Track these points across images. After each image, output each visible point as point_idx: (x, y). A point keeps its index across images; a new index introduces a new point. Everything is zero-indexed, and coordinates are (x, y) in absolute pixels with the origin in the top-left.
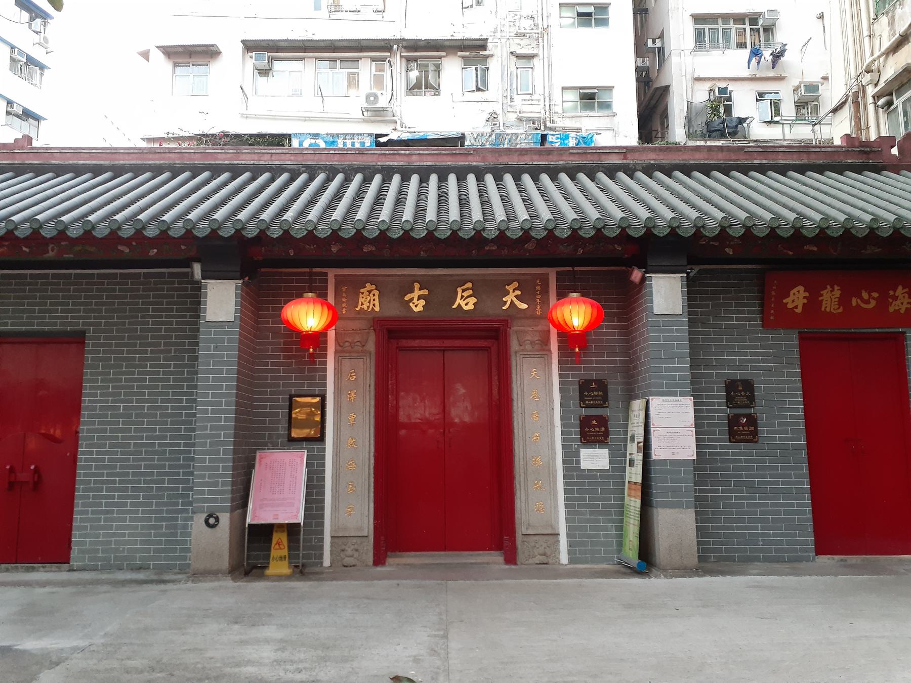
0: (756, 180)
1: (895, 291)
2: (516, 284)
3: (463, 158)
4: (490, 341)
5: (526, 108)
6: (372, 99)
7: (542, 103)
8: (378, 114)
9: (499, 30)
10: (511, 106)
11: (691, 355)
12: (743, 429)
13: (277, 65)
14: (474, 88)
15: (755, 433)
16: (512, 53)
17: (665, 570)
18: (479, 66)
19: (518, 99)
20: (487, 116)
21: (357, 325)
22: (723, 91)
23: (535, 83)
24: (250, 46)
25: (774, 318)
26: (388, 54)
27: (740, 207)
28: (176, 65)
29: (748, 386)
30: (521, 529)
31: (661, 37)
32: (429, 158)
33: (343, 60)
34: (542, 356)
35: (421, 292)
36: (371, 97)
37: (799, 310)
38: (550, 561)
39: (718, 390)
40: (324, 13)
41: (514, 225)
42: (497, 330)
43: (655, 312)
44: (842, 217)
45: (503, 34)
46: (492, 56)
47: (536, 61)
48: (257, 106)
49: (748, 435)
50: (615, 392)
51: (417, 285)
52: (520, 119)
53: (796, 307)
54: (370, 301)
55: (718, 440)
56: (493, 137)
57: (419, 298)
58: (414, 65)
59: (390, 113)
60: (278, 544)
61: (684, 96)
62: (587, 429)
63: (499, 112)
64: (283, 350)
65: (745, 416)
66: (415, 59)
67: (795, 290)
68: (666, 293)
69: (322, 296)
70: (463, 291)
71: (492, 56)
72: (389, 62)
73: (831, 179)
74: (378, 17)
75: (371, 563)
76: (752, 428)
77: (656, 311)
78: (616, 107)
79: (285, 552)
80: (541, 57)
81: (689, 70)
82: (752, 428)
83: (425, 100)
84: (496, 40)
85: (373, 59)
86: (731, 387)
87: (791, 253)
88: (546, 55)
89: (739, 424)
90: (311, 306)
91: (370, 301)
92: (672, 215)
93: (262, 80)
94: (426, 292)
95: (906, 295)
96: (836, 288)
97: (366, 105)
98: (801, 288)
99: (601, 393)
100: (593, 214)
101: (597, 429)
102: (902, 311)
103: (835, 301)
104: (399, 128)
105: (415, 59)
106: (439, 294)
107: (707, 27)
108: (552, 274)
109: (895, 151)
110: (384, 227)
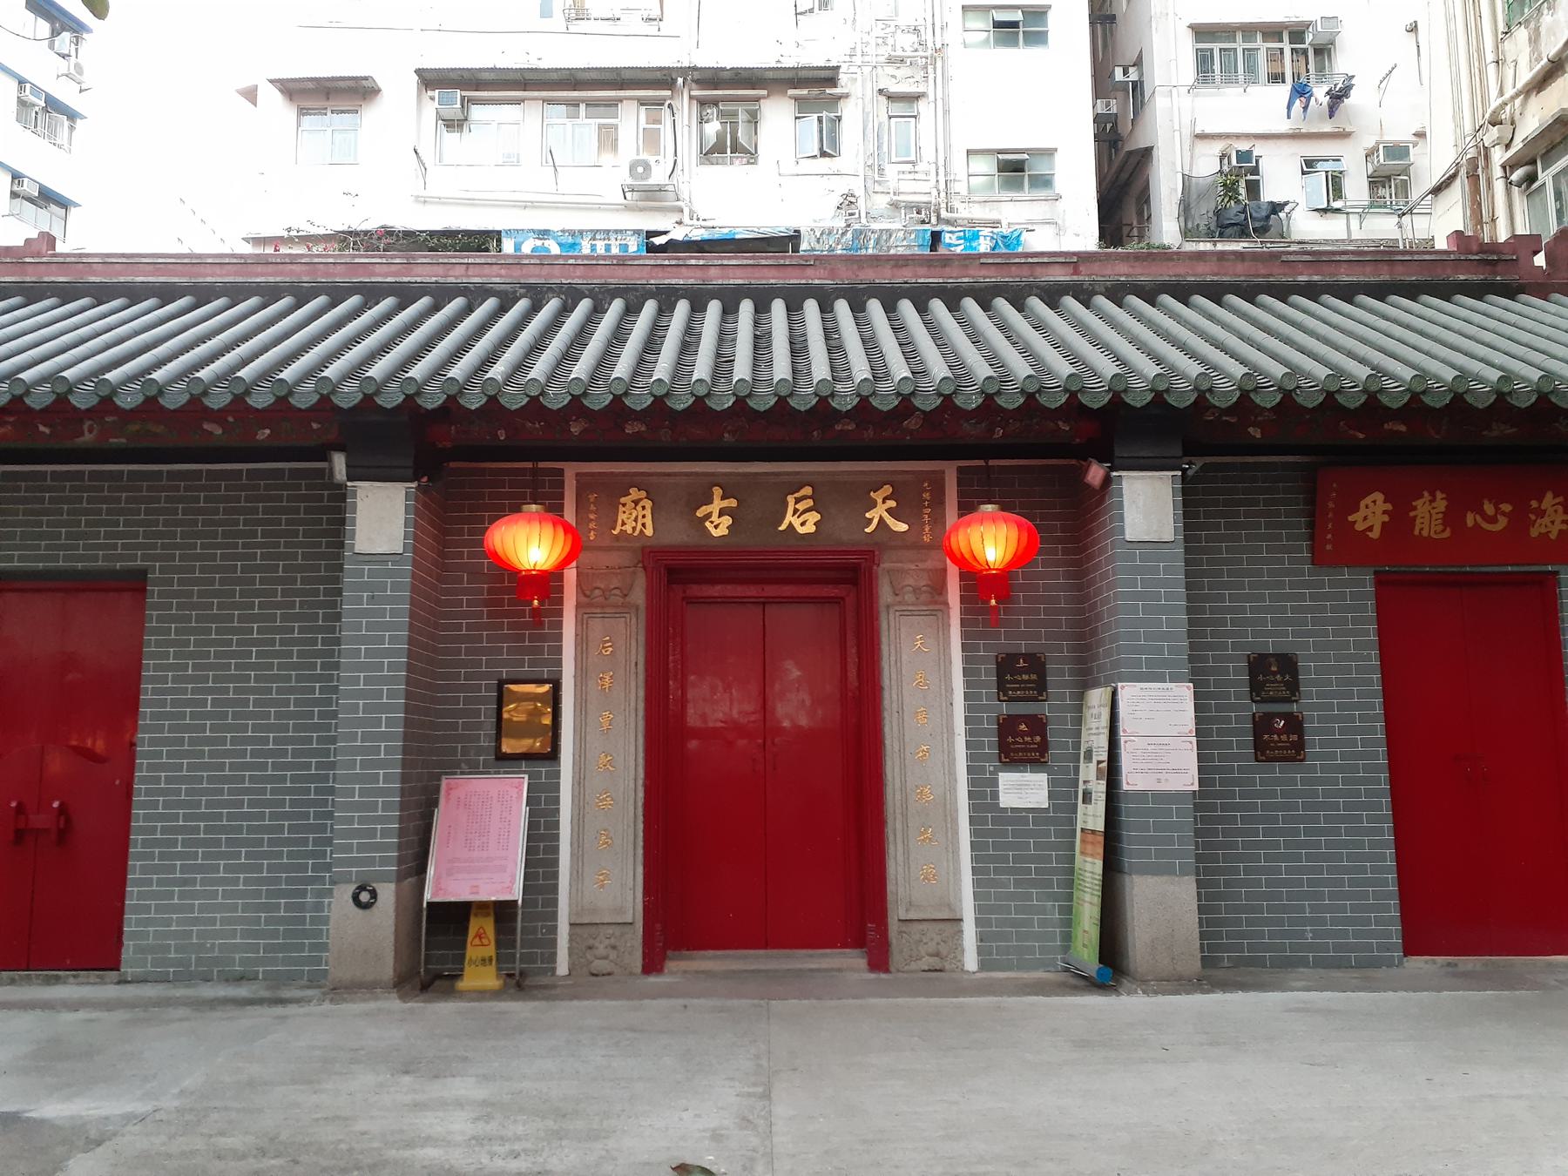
0: (1301, 309)
1: (1540, 501)
2: (888, 490)
3: (797, 272)
4: (844, 587)
5: (906, 186)
6: (640, 170)
7: (933, 177)
8: (650, 196)
9: (859, 53)
10: (879, 183)
11: (1189, 611)
12: (1279, 739)
13: (477, 112)
14: (816, 152)
15: (1299, 746)
16: (881, 91)
17: (1144, 982)
18: (824, 114)
19: (891, 171)
20: (838, 200)
21: (614, 559)
22: (1244, 156)
23: (921, 143)
24: (430, 80)
25: (1333, 547)
26: (668, 93)
27: (1274, 356)
28: (302, 112)
29: (1288, 664)
30: (897, 911)
31: (1138, 63)
32: (738, 272)
33: (590, 104)
34: (932, 613)
35: (725, 503)
36: (639, 168)
37: (1375, 534)
38: (947, 967)
39: (1236, 671)
40: (558, 22)
41: (884, 387)
42: (855, 568)
43: (1128, 538)
44: (1449, 374)
45: (866, 59)
46: (847, 96)
47: (922, 105)
48: (442, 182)
49: (1287, 748)
50: (1059, 674)
51: (717, 492)
52: (895, 205)
53: (1370, 529)
54: (636, 519)
55: (1236, 757)
56: (849, 235)
57: (722, 513)
58: (712, 111)
59: (671, 195)
60: (479, 936)
61: (1178, 166)
62: (1010, 739)
63: (859, 192)
64: (487, 603)
65: (1282, 716)
66: (715, 102)
67: (1368, 500)
68: (1146, 505)
69: (554, 509)
70: (798, 501)
71: (847, 96)
72: (670, 106)
73: (1430, 308)
74: (651, 29)
75: (639, 969)
76: (1294, 737)
77: (1130, 535)
78: (1060, 184)
79: (490, 951)
80: (931, 97)
81: (1186, 120)
82: (1294, 737)
83: (731, 173)
84: (853, 69)
85: (642, 102)
86: (1259, 666)
87: (1361, 436)
88: (939, 95)
89: (1272, 731)
90: (536, 527)
91: (636, 519)
92: (1157, 370)
93: (451, 138)
94: (733, 503)
95: (1560, 508)
96: (1439, 495)
97: (629, 181)
98: (1379, 496)
99: (1034, 677)
100: (1021, 369)
101: (1028, 739)
102: (1553, 536)
103: (1438, 518)
104: (686, 220)
105: (715, 102)
106: (755, 507)
107: (1216, 47)
108: (950, 471)
109: (1540, 260)
110: (660, 391)
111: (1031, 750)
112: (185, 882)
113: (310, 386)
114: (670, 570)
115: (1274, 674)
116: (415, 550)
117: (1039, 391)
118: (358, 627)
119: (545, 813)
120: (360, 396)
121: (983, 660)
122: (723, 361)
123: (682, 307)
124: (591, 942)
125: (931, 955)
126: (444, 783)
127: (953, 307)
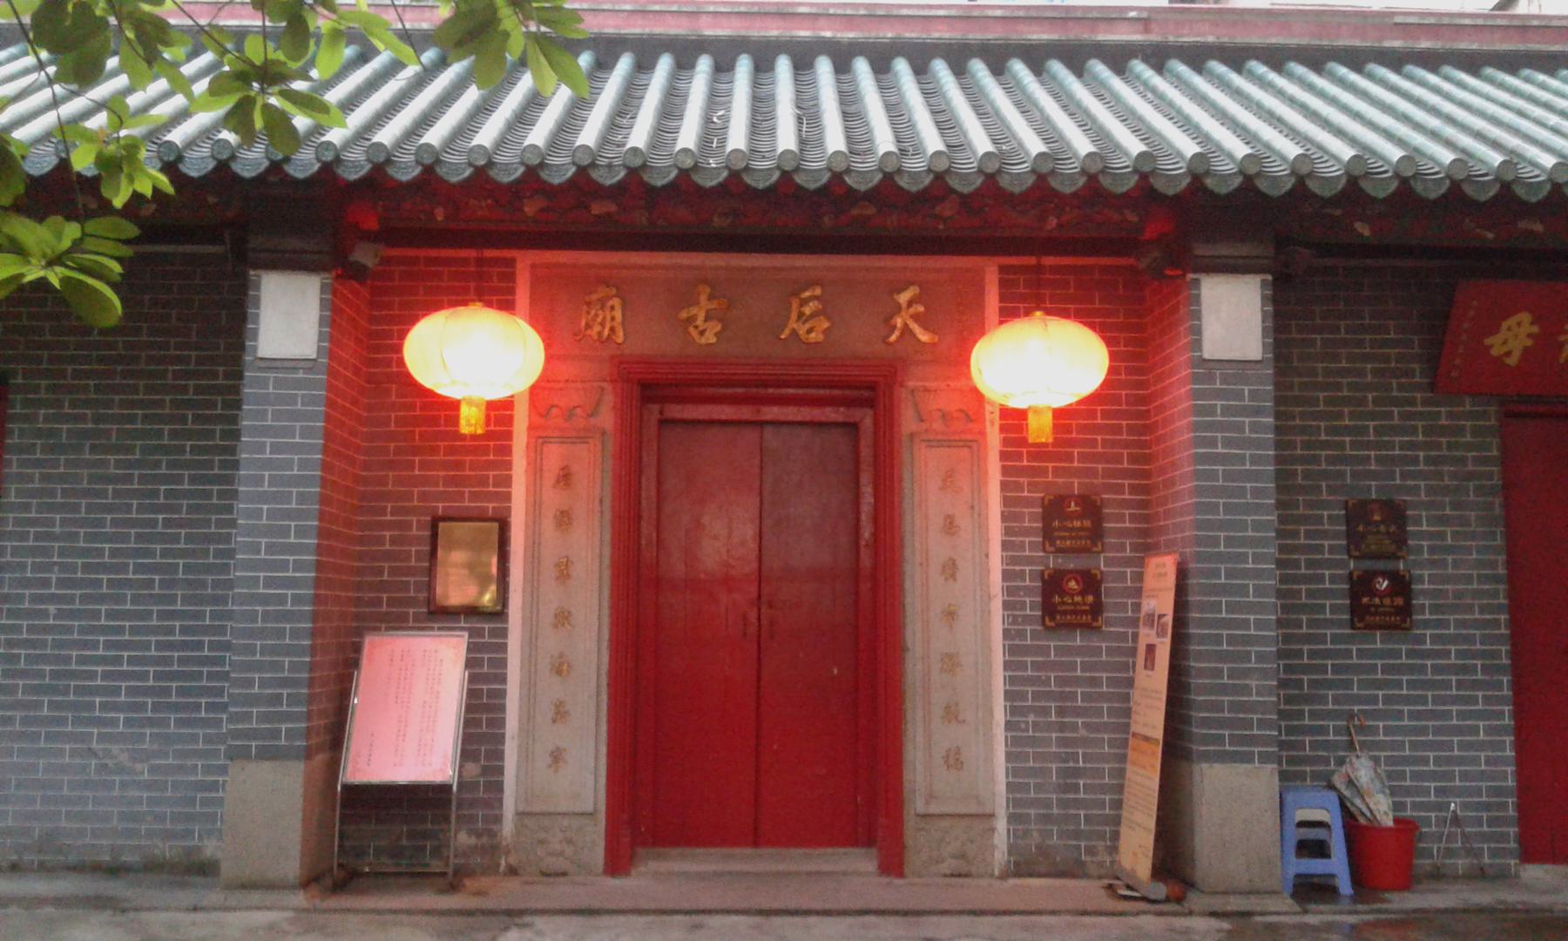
11: (1278, 445)
12: (1381, 603)
15: (1406, 611)
29: (1395, 513)
30: (916, 803)
41: (915, 164)
42: (872, 387)
43: (1206, 356)
49: (1391, 614)
50: (1119, 522)
53: (1508, 354)
62: (1057, 599)
67: (1512, 321)
68: (1230, 316)
76: (1400, 601)
77: (1210, 350)
82: (1400, 601)
86: (1357, 514)
87: (1490, 236)
89: (1373, 593)
99: (1087, 523)
101: (1078, 599)
111: (1085, 612)
112: (85, 645)
113: (205, 150)
114: (645, 386)
115: (1377, 523)
116: (332, 355)
117: (1102, 171)
118: (259, 480)
119: (488, 708)
120: (266, 163)
121: (1028, 502)
122: (712, 131)
123: (665, 64)
124: (542, 835)
125: (954, 857)
126: (369, 640)
127: (998, 70)
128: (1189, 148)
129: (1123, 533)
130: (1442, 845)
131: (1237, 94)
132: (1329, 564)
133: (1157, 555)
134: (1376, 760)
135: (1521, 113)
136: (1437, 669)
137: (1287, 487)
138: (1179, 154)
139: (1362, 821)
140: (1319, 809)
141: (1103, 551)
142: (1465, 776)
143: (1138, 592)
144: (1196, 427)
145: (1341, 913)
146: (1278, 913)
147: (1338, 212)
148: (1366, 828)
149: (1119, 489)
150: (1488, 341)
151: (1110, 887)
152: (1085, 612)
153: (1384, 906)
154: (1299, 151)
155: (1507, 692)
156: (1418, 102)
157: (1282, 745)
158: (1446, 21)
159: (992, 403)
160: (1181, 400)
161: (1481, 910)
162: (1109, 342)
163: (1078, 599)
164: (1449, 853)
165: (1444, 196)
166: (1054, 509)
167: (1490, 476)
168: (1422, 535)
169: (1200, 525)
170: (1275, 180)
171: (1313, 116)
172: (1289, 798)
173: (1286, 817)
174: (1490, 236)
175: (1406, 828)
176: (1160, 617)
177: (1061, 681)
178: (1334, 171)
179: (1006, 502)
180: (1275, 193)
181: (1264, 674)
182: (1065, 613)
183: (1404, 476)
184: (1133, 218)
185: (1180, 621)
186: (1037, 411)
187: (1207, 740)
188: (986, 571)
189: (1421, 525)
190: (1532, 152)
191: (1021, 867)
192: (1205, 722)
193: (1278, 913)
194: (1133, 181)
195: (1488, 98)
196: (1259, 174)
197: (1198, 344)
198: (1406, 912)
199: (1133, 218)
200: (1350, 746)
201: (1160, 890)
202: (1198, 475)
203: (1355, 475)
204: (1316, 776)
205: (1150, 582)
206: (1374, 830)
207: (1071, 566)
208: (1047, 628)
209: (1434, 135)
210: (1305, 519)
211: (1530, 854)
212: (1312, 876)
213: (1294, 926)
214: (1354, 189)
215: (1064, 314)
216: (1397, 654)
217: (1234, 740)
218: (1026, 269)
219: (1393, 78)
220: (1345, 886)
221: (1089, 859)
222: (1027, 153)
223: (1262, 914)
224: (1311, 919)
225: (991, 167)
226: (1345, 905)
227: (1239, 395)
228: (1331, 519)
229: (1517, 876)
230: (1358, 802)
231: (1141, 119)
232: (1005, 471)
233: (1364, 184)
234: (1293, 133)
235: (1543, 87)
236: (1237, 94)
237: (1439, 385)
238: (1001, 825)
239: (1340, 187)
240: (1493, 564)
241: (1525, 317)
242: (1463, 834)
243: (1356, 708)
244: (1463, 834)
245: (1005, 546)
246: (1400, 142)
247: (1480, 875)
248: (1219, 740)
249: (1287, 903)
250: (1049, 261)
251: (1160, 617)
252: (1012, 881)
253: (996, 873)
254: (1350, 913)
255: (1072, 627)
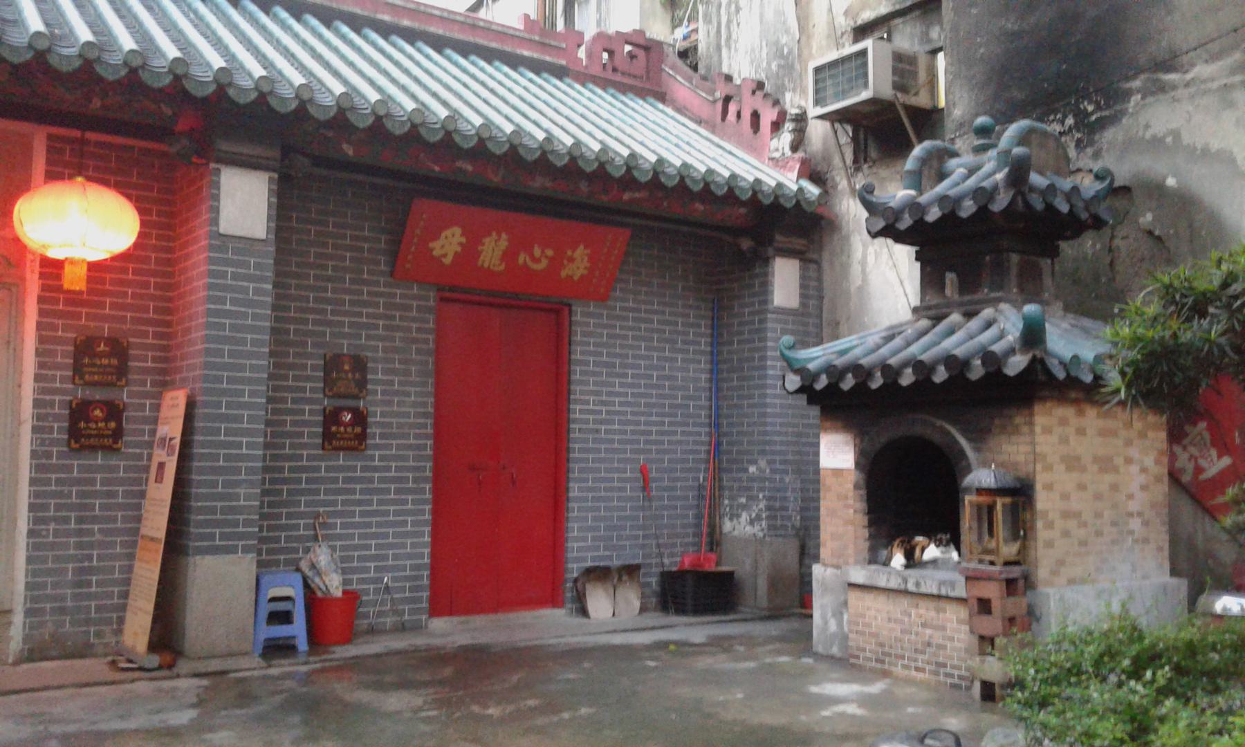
0: (401, 51)
1: (574, 251)
11: (275, 308)
12: (345, 431)
15: (362, 437)
25: (402, 258)
27: (371, 82)
29: (360, 365)
37: (448, 261)
43: (222, 231)
44: (509, 128)
50: (142, 362)
53: (445, 256)
62: (82, 425)
65: (350, 410)
67: (448, 233)
68: (243, 202)
76: (358, 430)
77: (225, 227)
82: (358, 430)
86: (332, 365)
87: (437, 169)
89: (339, 423)
96: (504, 236)
100: (127, 42)
101: (101, 425)
102: (576, 278)
103: (498, 253)
111: (108, 436)
115: (346, 372)
128: (217, 62)
129: (145, 371)
130: (377, 609)
131: (263, 29)
132: (310, 401)
133: (174, 389)
134: (333, 549)
135: (465, 85)
136: (381, 480)
137: (281, 341)
138: (208, 65)
139: (319, 594)
140: (288, 587)
141: (127, 384)
142: (396, 557)
143: (155, 421)
144: (210, 287)
145: (298, 664)
146: (248, 669)
147: (330, 134)
148: (321, 600)
149: (145, 334)
150: (431, 245)
151: (113, 663)
152: (108, 436)
153: (330, 657)
154: (303, 81)
155: (428, 496)
156: (397, 64)
157: (262, 540)
158: (422, 8)
159: (33, 253)
160: (199, 266)
161: (398, 653)
162: (141, 211)
163: (101, 425)
164: (380, 614)
165: (406, 134)
166: (84, 349)
167: (426, 341)
168: (377, 382)
169: (207, 365)
170: (283, 100)
171: (318, 57)
172: (265, 580)
173: (262, 592)
174: (437, 169)
175: (351, 598)
176: (171, 439)
177: (82, 495)
178: (329, 101)
179: (41, 340)
180: (281, 110)
181: (251, 484)
182: (90, 436)
183: (368, 337)
184: (167, 111)
185: (186, 443)
186: (72, 262)
187: (203, 537)
188: (18, 399)
189: (377, 375)
190: (467, 112)
191: (34, 653)
192: (200, 524)
193: (248, 669)
194: (167, 80)
195: (445, 70)
196: (271, 93)
197: (216, 221)
198: (345, 659)
199: (167, 111)
200: (316, 538)
201: (155, 660)
202: (209, 326)
203: (333, 334)
204: (287, 563)
205: (164, 412)
206: (328, 601)
207: (98, 397)
208: (72, 450)
209: (404, 89)
210: (292, 367)
211: (438, 608)
212: (279, 639)
213: (258, 678)
214: (341, 119)
215: (105, 183)
216: (354, 469)
217: (223, 536)
218: (73, 141)
219: (381, 42)
220: (302, 644)
221: (97, 641)
222: (76, 39)
223: (236, 671)
224: (274, 671)
225: (42, 45)
226: (302, 659)
227: (246, 265)
228: (313, 364)
229: (426, 627)
230: (317, 580)
231: (181, 32)
232: (42, 313)
233: (349, 115)
234: (301, 68)
235: (482, 70)
236: (263, 29)
237: (396, 273)
238: (18, 619)
239: (332, 114)
240: (425, 405)
241: (457, 231)
242: (392, 599)
243: (321, 510)
244: (392, 599)
245: (38, 378)
246: (379, 89)
247: (402, 628)
248: (212, 537)
249: (256, 661)
250: (91, 136)
251: (171, 439)
252: (25, 666)
253: (10, 661)
254: (306, 663)
255: (93, 448)
